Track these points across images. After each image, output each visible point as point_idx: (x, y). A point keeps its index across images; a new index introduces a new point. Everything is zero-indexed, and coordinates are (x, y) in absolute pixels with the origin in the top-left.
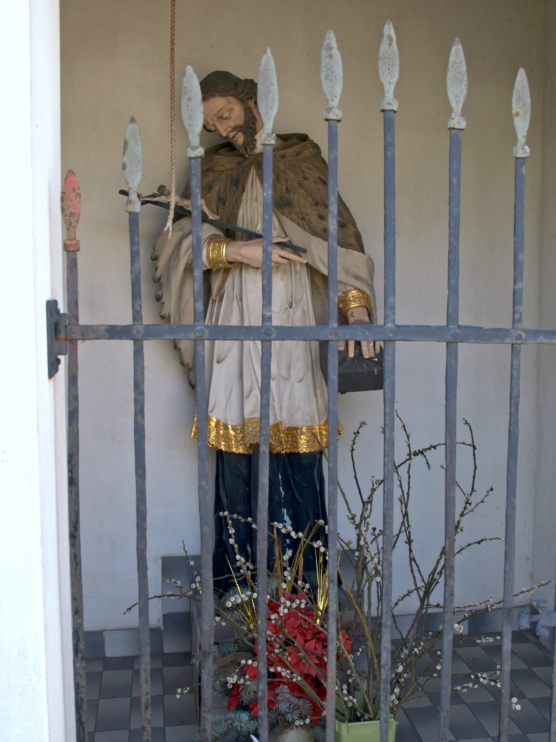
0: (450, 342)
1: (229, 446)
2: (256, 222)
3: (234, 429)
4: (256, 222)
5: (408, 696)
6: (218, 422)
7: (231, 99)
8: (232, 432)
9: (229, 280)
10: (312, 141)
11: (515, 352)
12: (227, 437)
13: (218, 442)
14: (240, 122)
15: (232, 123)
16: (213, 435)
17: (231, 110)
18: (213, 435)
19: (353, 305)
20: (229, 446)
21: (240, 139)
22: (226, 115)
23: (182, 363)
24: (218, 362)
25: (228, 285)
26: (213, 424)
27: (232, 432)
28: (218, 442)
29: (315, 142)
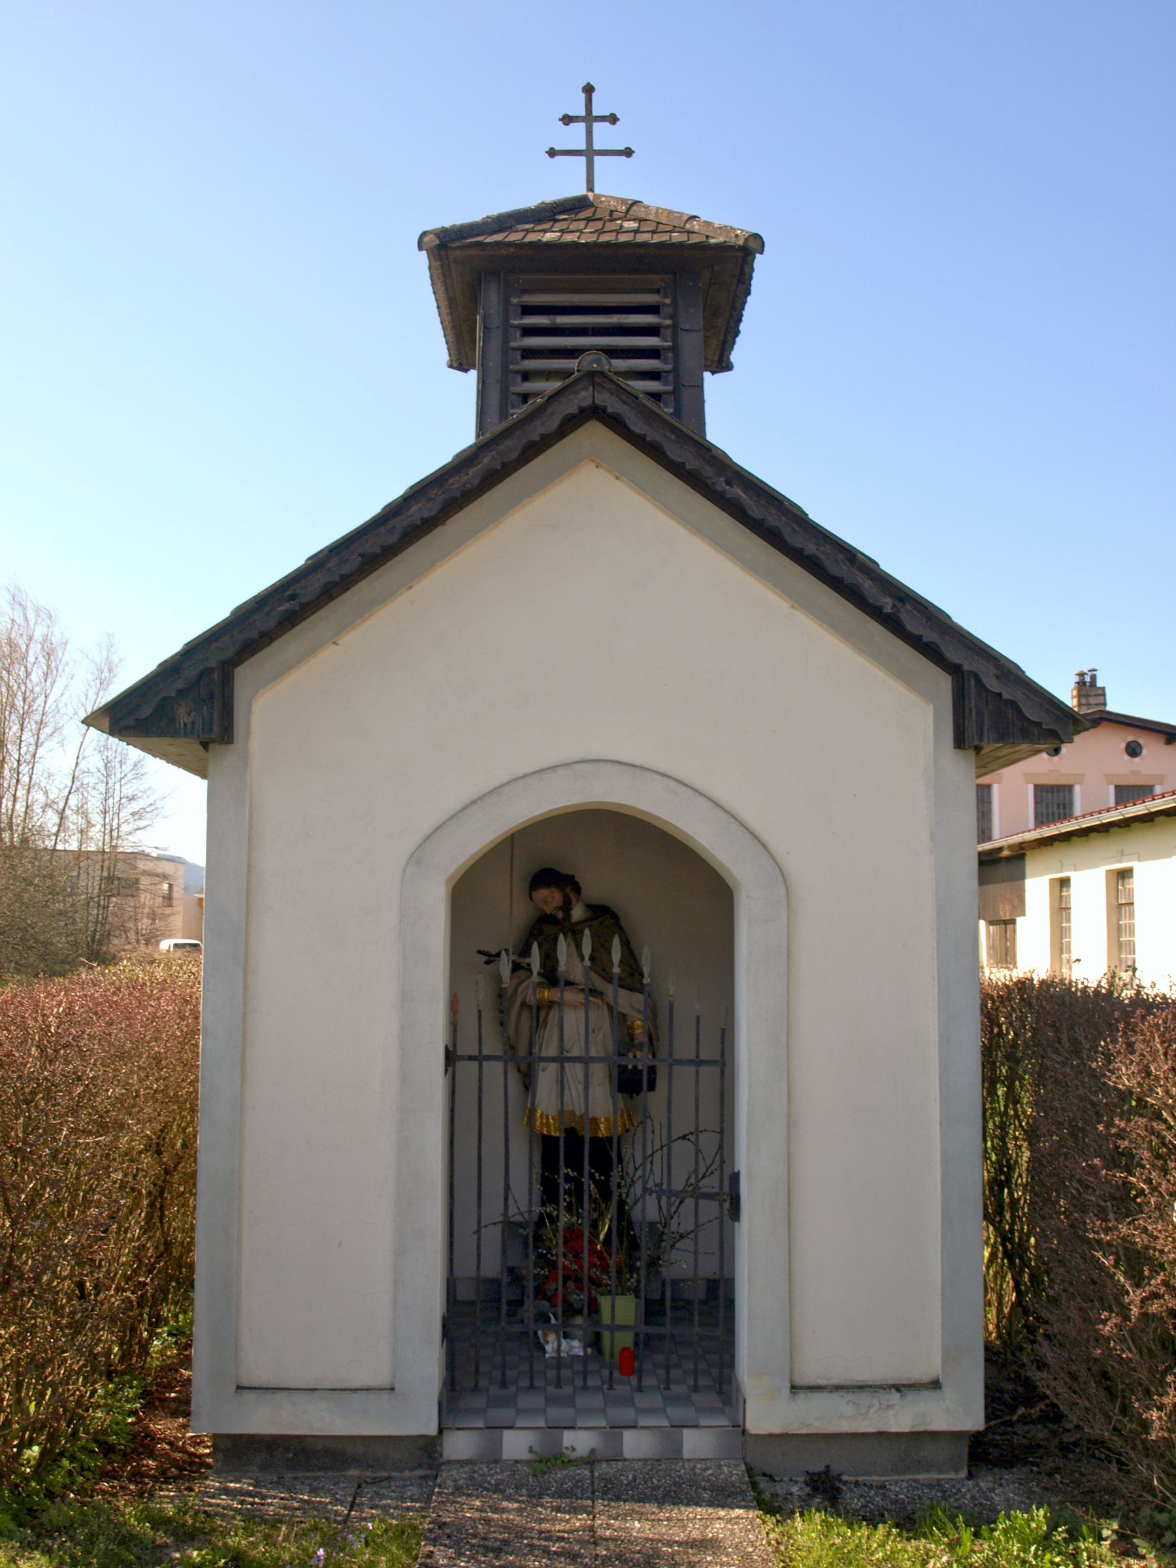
0: (722, 1072)
1: (549, 1131)
2: (473, 252)
3: (553, 1119)
4: (473, 252)
5: (619, 1186)
6: (542, 1114)
7: (553, 889)
8: (551, 1121)
9: (552, 1013)
10: (737, 333)
11: (671, 1055)
12: (548, 1125)
13: (542, 1128)
14: (560, 904)
15: (554, 905)
16: (538, 1122)
17: (553, 897)
18: (538, 1122)
19: (638, 1031)
20: (549, 1131)
21: (560, 915)
22: (550, 900)
23: (519, 1071)
24: (543, 1070)
25: (551, 1016)
26: (538, 1115)
27: (551, 1121)
28: (542, 1128)
29: (753, 282)
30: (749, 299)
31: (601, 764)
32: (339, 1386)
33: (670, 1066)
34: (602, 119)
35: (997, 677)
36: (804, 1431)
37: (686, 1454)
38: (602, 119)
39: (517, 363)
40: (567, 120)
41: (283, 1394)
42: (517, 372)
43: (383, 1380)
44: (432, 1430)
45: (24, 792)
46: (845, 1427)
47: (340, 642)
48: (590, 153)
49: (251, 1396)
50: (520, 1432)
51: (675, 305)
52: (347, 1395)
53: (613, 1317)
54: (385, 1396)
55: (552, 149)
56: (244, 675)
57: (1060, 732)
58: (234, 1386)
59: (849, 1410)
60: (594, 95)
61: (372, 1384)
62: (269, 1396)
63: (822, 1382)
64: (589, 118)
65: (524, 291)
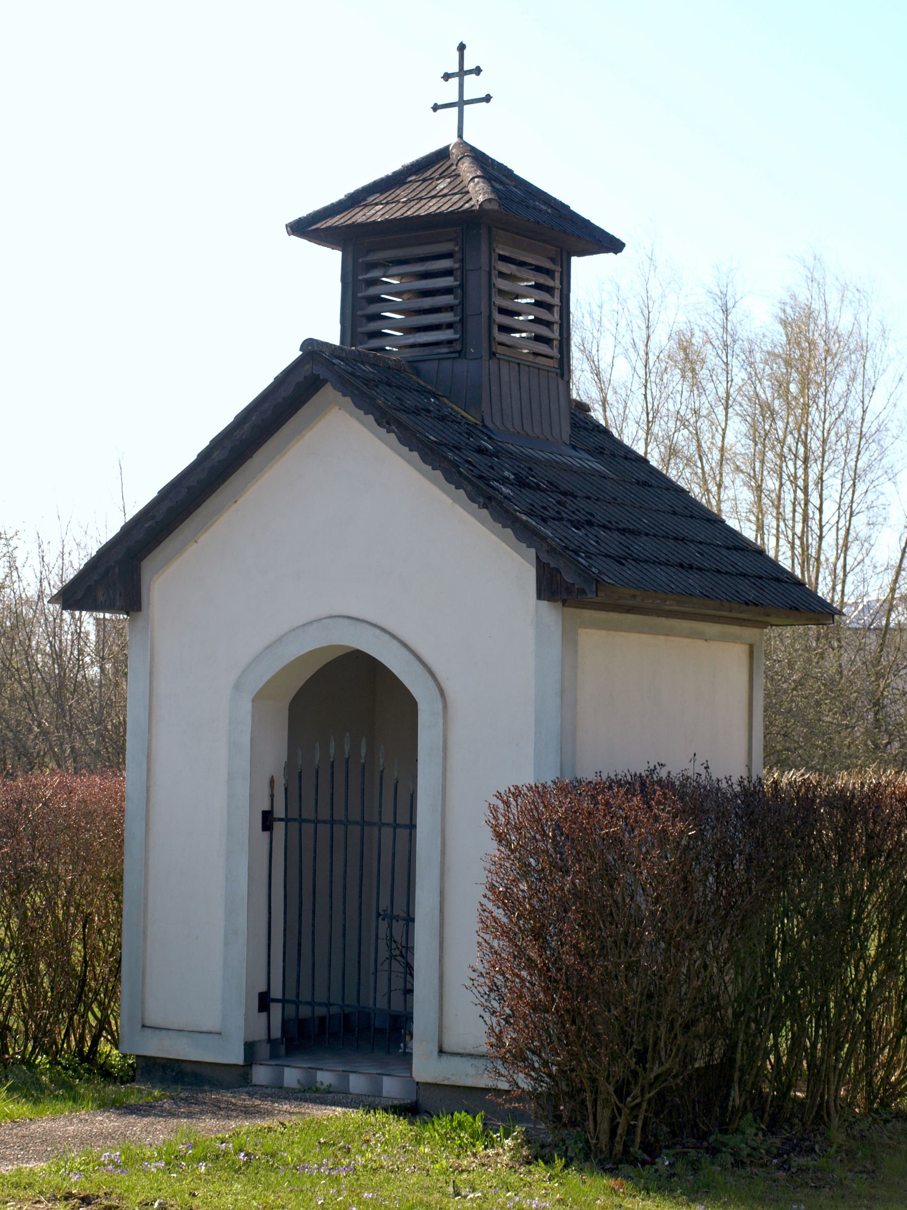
30: (572, 208)
31: (337, 619)
32: (196, 1029)
33: (300, 823)
34: (470, 72)
35: (548, 552)
36: (446, 1083)
37: (385, 1094)
38: (470, 72)
39: (362, 309)
40: (447, 77)
41: (165, 1032)
42: (361, 316)
43: (216, 1027)
44: (240, 1060)
45: (812, 499)
46: (469, 1082)
47: (199, 541)
48: (461, 103)
49: (148, 1032)
50: (293, 1070)
51: (462, 250)
52: (196, 1035)
53: (375, 1004)
54: (217, 1037)
55: (436, 104)
56: (148, 566)
57: (587, 590)
58: (140, 1026)
59: (472, 1071)
60: (465, 51)
61: (212, 1030)
62: (157, 1032)
63: (461, 1051)
64: (462, 73)
65: (369, 251)
